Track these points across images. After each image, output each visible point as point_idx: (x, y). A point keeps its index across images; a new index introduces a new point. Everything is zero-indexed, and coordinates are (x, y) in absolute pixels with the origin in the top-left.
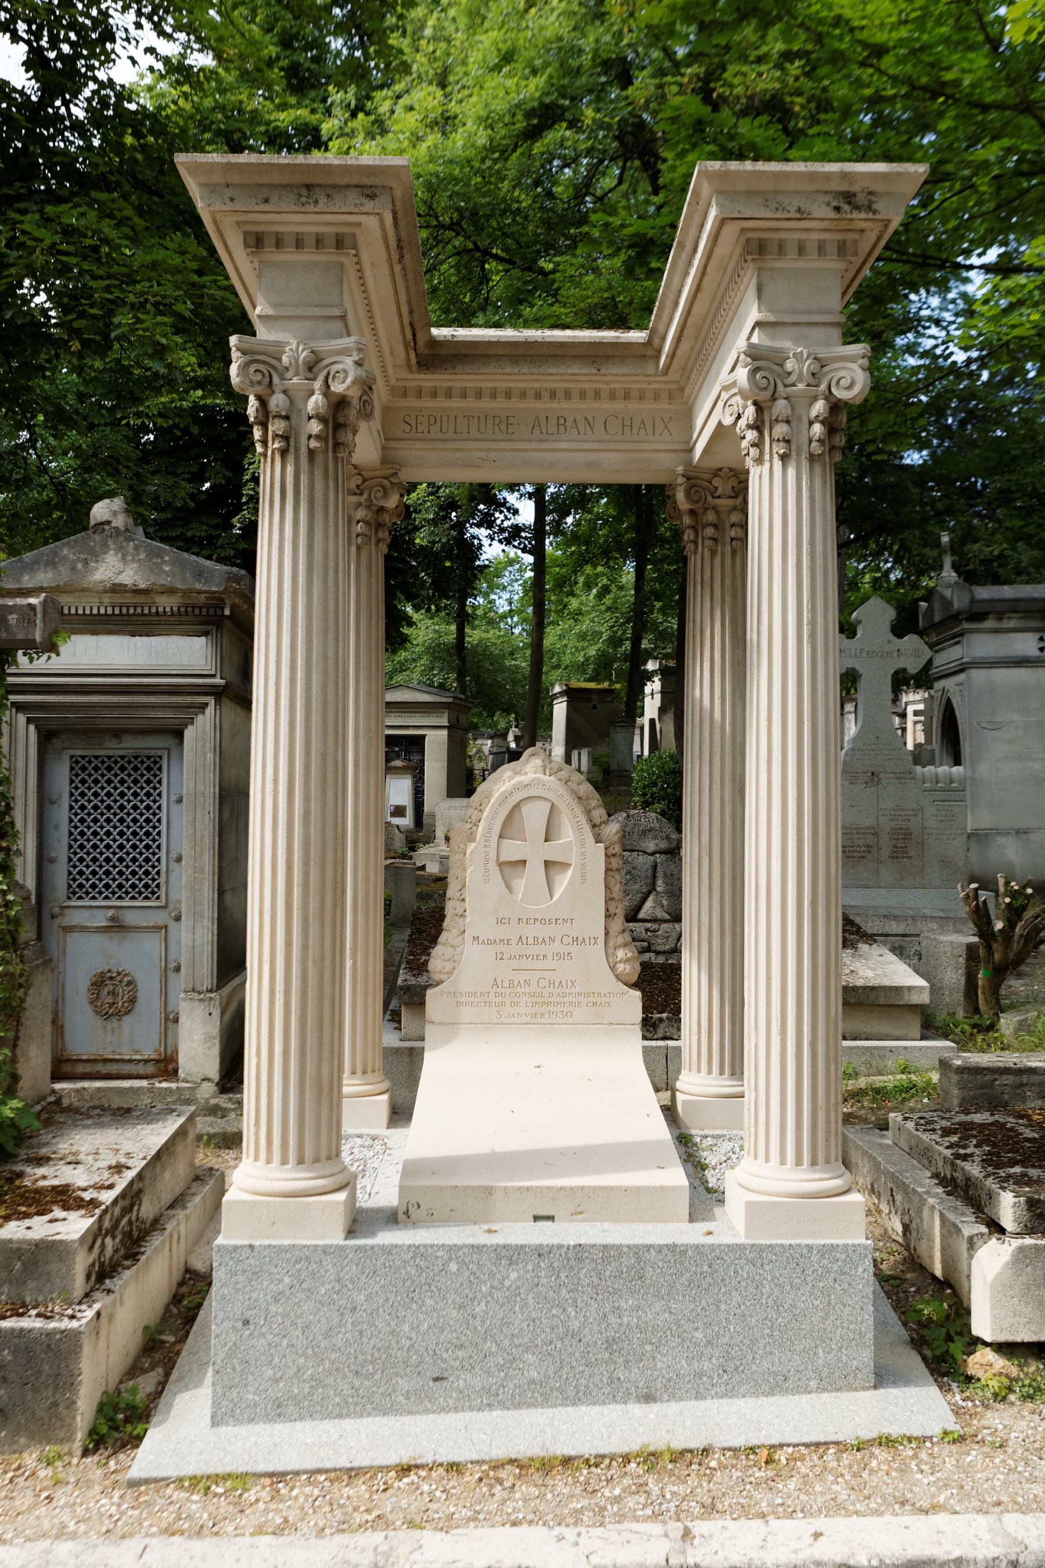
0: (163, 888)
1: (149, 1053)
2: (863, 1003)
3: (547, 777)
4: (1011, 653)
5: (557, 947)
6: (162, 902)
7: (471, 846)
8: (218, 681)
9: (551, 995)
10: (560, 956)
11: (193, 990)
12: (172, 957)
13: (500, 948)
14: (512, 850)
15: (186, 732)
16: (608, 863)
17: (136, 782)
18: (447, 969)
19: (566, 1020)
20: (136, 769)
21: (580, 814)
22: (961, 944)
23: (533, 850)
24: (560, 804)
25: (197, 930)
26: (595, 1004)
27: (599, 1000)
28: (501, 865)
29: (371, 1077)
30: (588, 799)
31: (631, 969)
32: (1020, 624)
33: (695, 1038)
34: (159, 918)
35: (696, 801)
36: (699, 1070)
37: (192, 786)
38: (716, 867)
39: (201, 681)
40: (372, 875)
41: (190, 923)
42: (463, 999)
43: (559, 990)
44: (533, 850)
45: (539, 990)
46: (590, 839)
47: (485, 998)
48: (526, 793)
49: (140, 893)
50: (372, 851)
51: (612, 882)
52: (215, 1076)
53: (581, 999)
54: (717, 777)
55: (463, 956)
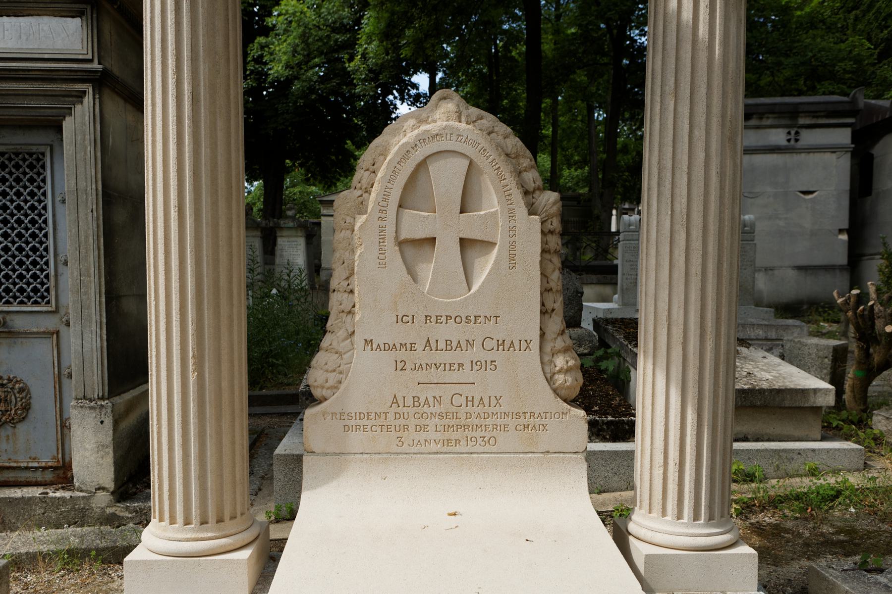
0: (53, 293)
1: (46, 460)
2: (758, 407)
3: (463, 125)
4: (767, 144)
5: (476, 353)
6: (54, 309)
7: (361, 220)
8: (95, 66)
9: (468, 415)
10: (480, 365)
11: (85, 397)
12: (64, 364)
13: (402, 354)
14: (416, 224)
15: (64, 124)
16: (544, 243)
17: (18, 180)
18: (331, 382)
19: (487, 448)
20: (17, 167)
21: (507, 175)
22: (828, 347)
23: (442, 223)
24: (482, 162)
25: (85, 335)
26: (526, 427)
27: (531, 422)
28: (402, 244)
29: (229, 526)
30: (517, 156)
31: (571, 381)
32: (776, 122)
33: (658, 472)
34: (49, 323)
35: (669, 155)
36: (664, 513)
37: (73, 182)
38: (696, 244)
39: (75, 66)
40: (223, 257)
41: (79, 328)
42: (353, 422)
43: (478, 410)
44: (442, 223)
45: (454, 409)
46: (521, 209)
47: (382, 421)
48: (435, 147)
49: (29, 298)
50: (222, 223)
51: (550, 267)
52: (111, 486)
53: (508, 420)
54: (700, 119)
55: (353, 369)
